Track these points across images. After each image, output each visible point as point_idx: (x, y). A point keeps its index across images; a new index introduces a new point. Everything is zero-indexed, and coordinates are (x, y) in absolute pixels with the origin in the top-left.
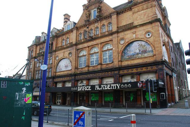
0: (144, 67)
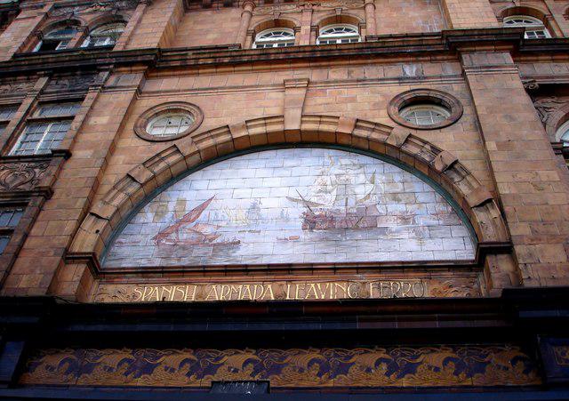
0: (368, 340)
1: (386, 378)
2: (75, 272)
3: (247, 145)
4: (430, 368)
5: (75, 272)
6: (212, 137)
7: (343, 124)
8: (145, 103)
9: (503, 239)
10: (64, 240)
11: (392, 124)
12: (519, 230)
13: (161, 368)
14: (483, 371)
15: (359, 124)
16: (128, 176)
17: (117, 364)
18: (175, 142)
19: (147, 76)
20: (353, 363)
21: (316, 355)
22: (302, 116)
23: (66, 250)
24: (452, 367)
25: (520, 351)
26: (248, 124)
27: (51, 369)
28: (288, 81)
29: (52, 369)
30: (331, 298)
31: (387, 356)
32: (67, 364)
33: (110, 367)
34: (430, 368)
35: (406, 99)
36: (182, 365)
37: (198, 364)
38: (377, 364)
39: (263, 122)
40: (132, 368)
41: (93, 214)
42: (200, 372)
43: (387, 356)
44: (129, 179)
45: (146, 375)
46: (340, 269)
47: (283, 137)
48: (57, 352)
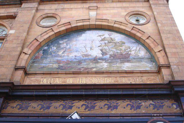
0: (79, 97)
1: (130, 110)
2: (20, 73)
3: (100, 27)
4: (77, 107)
5: (20, 73)
6: (64, 26)
7: (111, 23)
8: (39, 14)
9: (167, 63)
10: (14, 63)
11: (127, 23)
12: (173, 60)
13: (53, 107)
14: (117, 108)
15: (116, 22)
16: (36, 39)
17: (59, 106)
18: (52, 28)
19: (39, 4)
20: (96, 106)
21: (106, 102)
22: (96, 19)
23: (15, 66)
24: (152, 107)
25: (175, 101)
26: (115, 22)
27: (14, 108)
28: (90, 7)
29: (13, 108)
30: (71, 83)
31: (108, 103)
32: (62, 106)
33: (35, 107)
34: (77, 107)
35: (44, 17)
36: (60, 106)
37: (65, 106)
38: (60, 106)
39: (82, 21)
40: (64, 107)
41: (24, 53)
42: (135, 108)
43: (130, 103)
44: (36, 40)
45: (115, 110)
46: (90, 73)
47: (89, 26)
48: (14, 102)
